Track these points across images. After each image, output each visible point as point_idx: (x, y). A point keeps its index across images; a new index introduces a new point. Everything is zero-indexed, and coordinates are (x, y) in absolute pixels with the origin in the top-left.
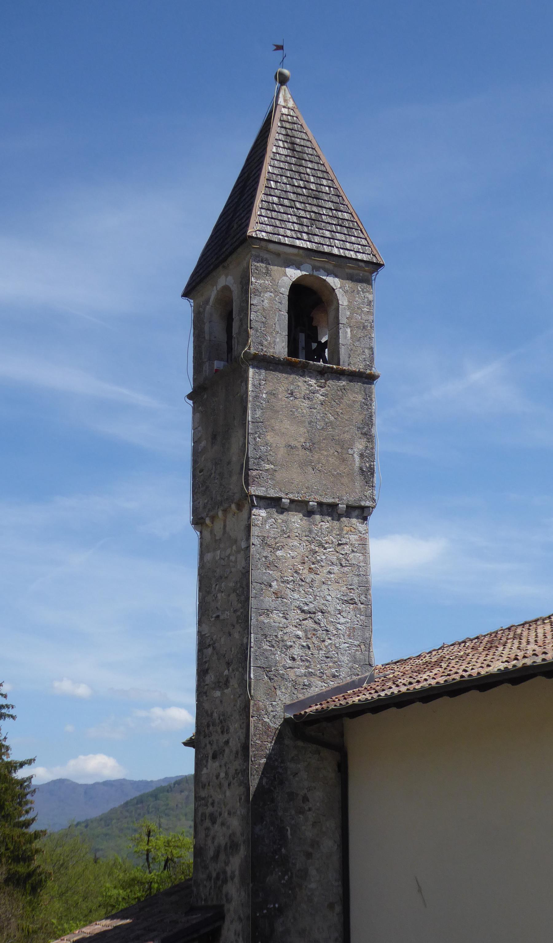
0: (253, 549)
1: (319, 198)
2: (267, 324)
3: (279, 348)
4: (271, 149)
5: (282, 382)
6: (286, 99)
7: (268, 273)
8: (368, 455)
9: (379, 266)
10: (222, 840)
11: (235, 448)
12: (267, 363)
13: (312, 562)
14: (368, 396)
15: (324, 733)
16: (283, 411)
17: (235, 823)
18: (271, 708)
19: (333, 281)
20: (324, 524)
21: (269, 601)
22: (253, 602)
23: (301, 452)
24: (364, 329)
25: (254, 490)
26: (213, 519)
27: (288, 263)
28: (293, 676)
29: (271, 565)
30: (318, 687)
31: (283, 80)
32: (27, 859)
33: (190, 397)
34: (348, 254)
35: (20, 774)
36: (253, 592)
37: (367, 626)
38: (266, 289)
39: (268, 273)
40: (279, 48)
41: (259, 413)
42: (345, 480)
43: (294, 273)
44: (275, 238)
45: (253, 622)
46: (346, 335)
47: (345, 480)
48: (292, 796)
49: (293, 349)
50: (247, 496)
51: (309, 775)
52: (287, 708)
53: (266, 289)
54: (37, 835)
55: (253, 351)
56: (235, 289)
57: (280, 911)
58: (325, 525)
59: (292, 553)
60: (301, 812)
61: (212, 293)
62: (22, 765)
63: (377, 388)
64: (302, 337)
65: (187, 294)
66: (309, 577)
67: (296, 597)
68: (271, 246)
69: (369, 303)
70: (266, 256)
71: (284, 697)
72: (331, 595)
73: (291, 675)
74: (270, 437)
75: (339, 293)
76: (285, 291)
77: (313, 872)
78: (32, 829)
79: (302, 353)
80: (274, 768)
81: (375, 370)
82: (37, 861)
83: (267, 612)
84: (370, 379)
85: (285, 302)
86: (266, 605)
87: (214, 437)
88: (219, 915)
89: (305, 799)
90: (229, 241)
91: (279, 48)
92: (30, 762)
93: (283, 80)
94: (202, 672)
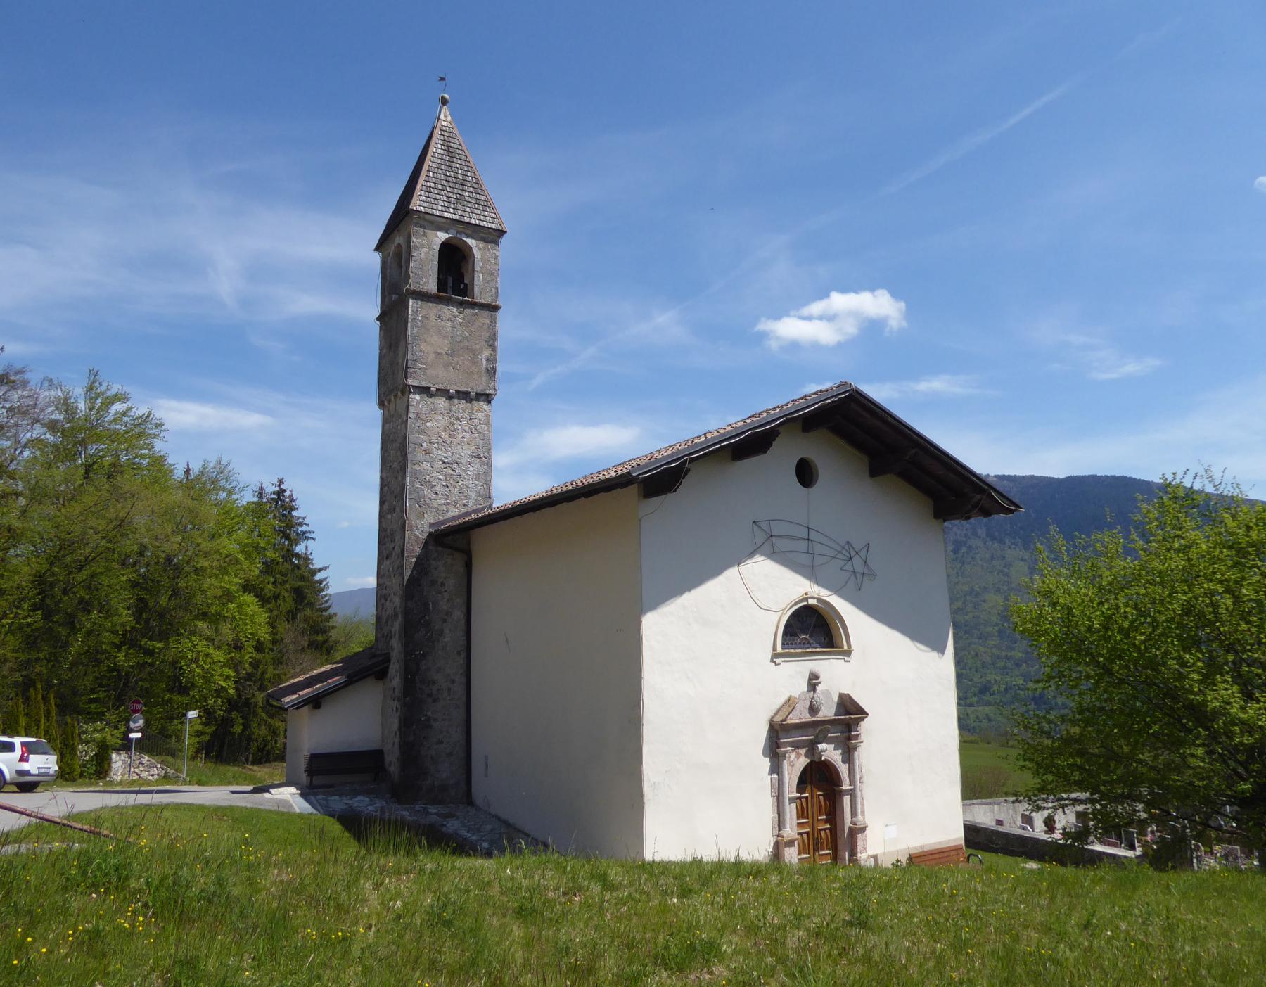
0: (410, 421)
1: (464, 184)
2: (434, 271)
3: (431, 285)
4: (432, 149)
5: (433, 310)
6: (445, 116)
7: (424, 235)
8: (492, 360)
9: (503, 232)
10: (390, 611)
11: (401, 354)
12: (422, 296)
13: (451, 430)
14: (494, 320)
15: (456, 540)
16: (433, 328)
17: (397, 600)
18: (420, 526)
19: (471, 242)
20: (461, 405)
21: (420, 455)
22: (409, 456)
23: (445, 357)
24: (493, 274)
25: (410, 382)
26: (389, 402)
27: (440, 228)
28: (438, 503)
29: (422, 432)
30: (453, 512)
31: (444, 102)
32: (324, 631)
33: (378, 319)
34: (482, 223)
35: (318, 577)
36: (409, 450)
37: (488, 473)
38: (423, 246)
39: (424, 235)
40: (443, 79)
41: (416, 330)
42: (476, 376)
43: (443, 236)
44: (430, 211)
45: (409, 469)
46: (479, 279)
47: (476, 376)
48: (433, 583)
49: (442, 285)
50: (406, 386)
51: (446, 570)
52: (431, 525)
53: (423, 246)
54: (331, 617)
55: (412, 288)
56: (404, 247)
57: (424, 656)
58: (461, 406)
59: (438, 423)
60: (440, 593)
61: (392, 249)
62: (320, 570)
63: (499, 314)
64: (450, 280)
65: (377, 249)
66: (449, 440)
67: (439, 453)
68: (427, 217)
69: (496, 257)
70: (421, 222)
71: (429, 518)
72: (464, 453)
73: (435, 505)
74: (423, 347)
75: (475, 250)
76: (437, 247)
77: (447, 631)
78: (331, 611)
79: (450, 290)
80: (422, 564)
81: (499, 303)
82: (333, 633)
83: (419, 463)
84: (495, 308)
85: (437, 255)
86: (418, 458)
87: (390, 347)
88: (387, 660)
89: (442, 584)
90: (402, 216)
91: (443, 79)
92: (326, 568)
93: (444, 102)
94: (382, 503)
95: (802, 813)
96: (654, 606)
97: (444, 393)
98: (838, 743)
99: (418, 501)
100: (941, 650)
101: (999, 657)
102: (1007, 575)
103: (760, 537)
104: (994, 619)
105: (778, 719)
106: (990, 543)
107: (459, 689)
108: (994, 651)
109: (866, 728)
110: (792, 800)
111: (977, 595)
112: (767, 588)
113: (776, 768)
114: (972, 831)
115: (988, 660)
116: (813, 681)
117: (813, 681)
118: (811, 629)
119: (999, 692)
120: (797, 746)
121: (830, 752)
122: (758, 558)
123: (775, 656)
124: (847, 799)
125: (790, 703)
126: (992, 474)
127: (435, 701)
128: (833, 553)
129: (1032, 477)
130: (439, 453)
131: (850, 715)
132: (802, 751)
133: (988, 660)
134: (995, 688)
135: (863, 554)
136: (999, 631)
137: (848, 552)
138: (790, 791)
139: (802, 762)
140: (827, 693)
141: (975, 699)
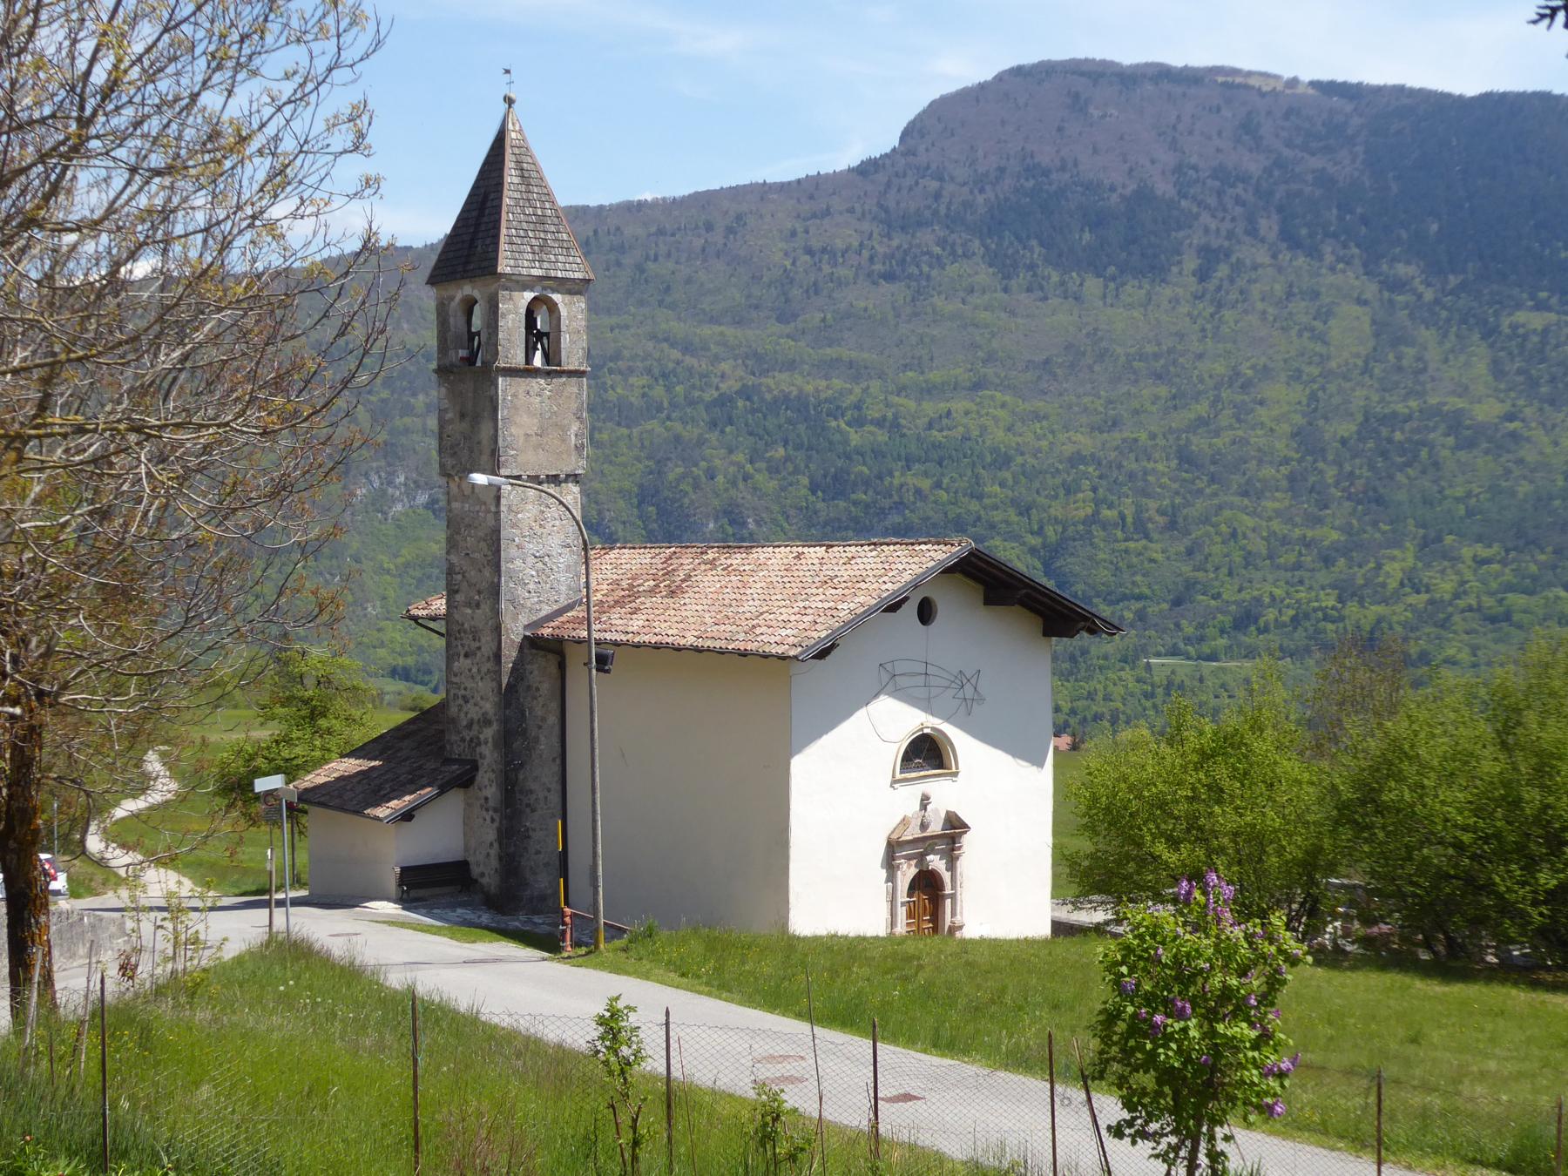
3: (518, 359)
12: (512, 372)
13: (541, 520)
19: (557, 297)
29: (514, 526)
38: (509, 312)
40: (508, 72)
43: (529, 296)
48: (529, 687)
51: (540, 674)
57: (522, 765)
59: (528, 514)
71: (524, 619)
74: (513, 430)
77: (542, 739)
83: (512, 560)
89: (538, 689)
91: (508, 72)
95: (910, 915)
96: (799, 751)
97: (535, 479)
98: (942, 854)
99: (512, 602)
100: (1040, 764)
101: (1285, 541)
102: (1321, 338)
103: (885, 677)
104: (1281, 447)
105: (895, 836)
106: (1285, 256)
107: (555, 798)
108: (1276, 525)
109: (967, 841)
110: (903, 904)
111: (1245, 387)
112: (893, 720)
113: (891, 878)
114: (1059, 928)
115: (1259, 546)
116: (925, 801)
117: (925, 801)
118: (926, 753)
119: (1279, 625)
120: (909, 858)
121: (936, 862)
122: (882, 697)
123: (895, 782)
124: (948, 902)
125: (905, 822)
126: (1306, 77)
127: (533, 811)
128: (947, 683)
129: (1400, 90)
130: (531, 547)
131: (955, 827)
132: (913, 862)
133: (1259, 546)
134: (1271, 615)
135: (973, 681)
136: (1292, 478)
137: (960, 680)
138: (902, 897)
139: (913, 871)
140: (936, 811)
141: (1222, 642)
